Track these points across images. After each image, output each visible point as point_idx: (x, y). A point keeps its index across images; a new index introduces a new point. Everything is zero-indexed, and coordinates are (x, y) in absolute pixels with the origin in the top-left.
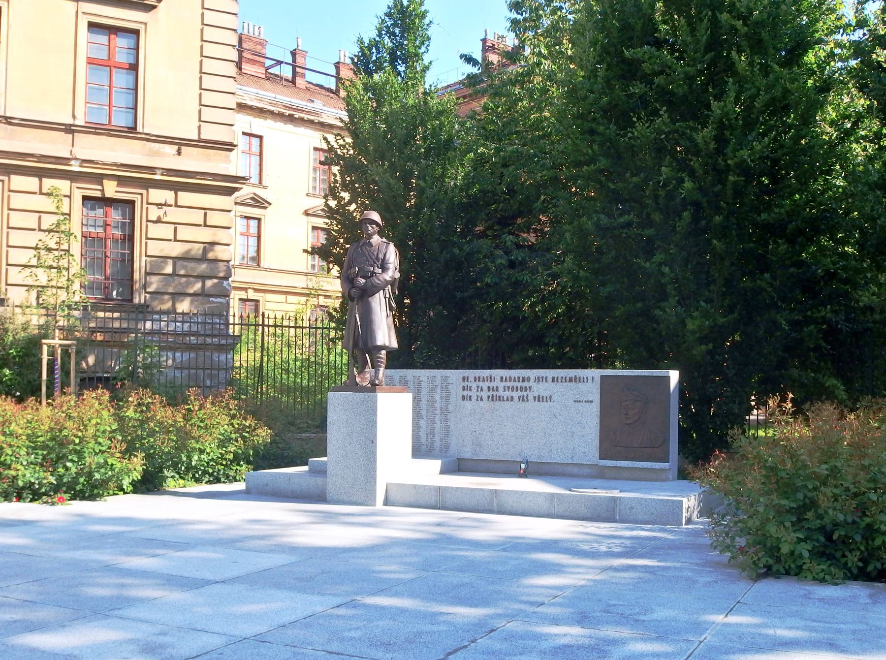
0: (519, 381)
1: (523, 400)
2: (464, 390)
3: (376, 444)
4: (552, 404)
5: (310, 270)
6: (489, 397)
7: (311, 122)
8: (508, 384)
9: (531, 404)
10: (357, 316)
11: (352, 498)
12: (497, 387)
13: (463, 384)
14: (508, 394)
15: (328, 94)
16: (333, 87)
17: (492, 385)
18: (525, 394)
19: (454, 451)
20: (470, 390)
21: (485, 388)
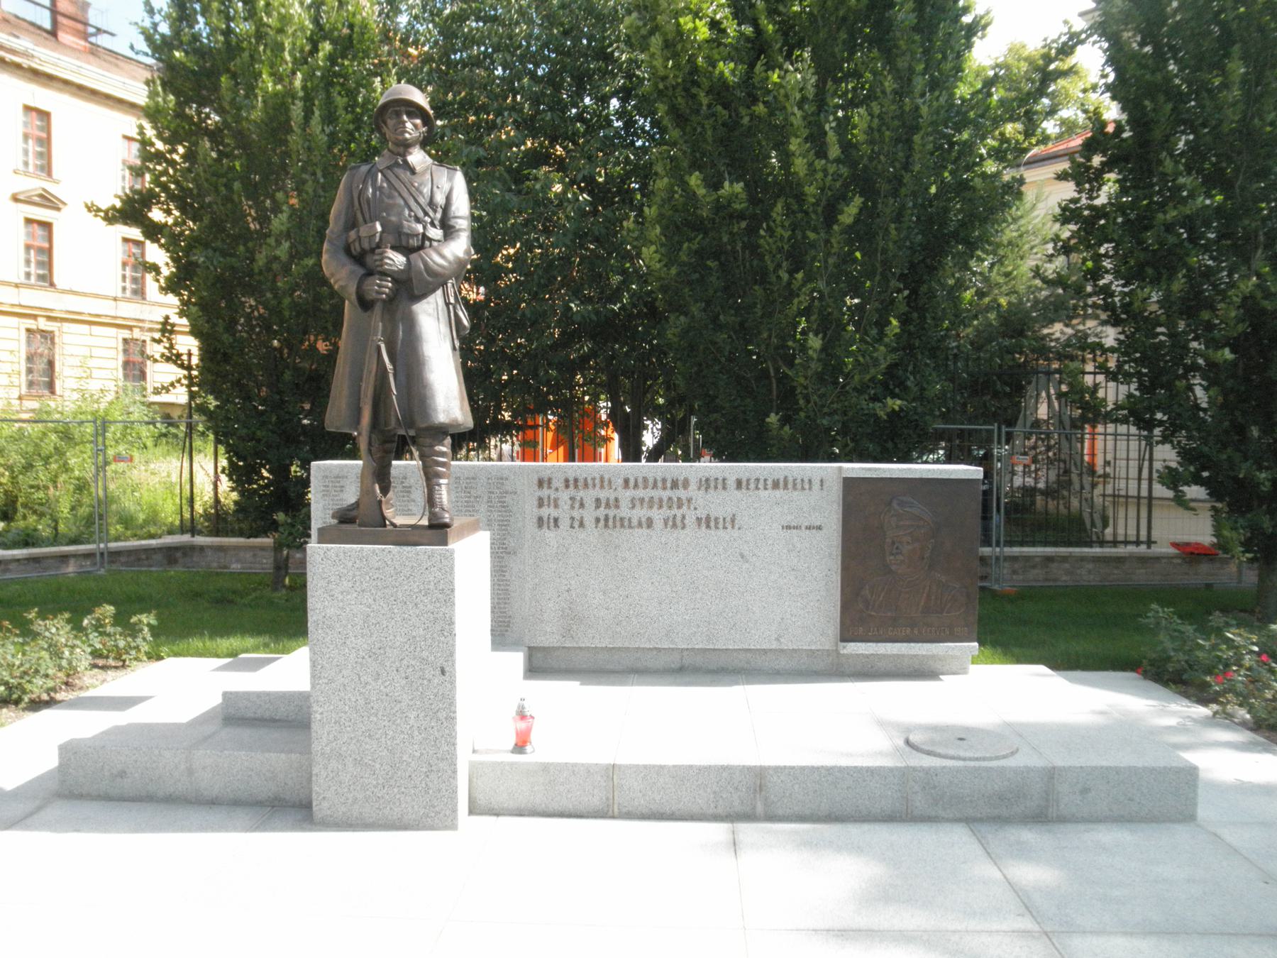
0: (665, 488)
1: (674, 525)
2: (541, 505)
3: (453, 676)
4: (736, 533)
5: (22, 279)
6: (598, 520)
7: (18, 66)
8: (640, 493)
9: (690, 534)
10: (383, 346)
11: (387, 811)
12: (617, 500)
13: (539, 493)
14: (640, 513)
15: (39, 32)
16: (47, 24)
17: (603, 494)
18: (679, 513)
19: (549, 636)
20: (556, 506)
21: (590, 503)
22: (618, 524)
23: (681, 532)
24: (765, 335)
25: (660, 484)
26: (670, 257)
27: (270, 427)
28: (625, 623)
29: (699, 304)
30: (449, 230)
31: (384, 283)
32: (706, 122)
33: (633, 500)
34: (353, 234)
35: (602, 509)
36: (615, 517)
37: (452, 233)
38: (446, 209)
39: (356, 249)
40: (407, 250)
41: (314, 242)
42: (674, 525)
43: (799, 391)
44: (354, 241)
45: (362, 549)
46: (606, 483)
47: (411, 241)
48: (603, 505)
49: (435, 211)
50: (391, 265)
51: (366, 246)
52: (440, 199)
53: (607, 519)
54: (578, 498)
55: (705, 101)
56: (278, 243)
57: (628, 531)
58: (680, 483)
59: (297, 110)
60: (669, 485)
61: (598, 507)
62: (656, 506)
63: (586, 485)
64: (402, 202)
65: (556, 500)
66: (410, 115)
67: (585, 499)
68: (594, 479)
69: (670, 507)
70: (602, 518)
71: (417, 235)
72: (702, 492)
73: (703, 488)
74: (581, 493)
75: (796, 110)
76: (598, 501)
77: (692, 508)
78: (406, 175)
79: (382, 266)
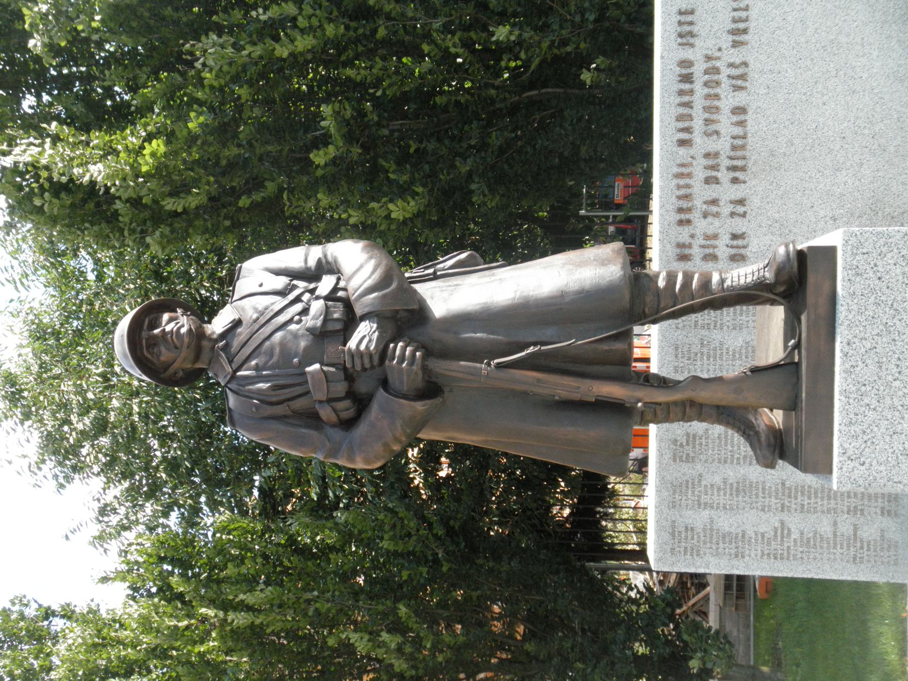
0: (691, 92)
6: (735, 181)
8: (698, 125)
12: (707, 155)
14: (725, 124)
17: (700, 174)
18: (726, 71)
20: (715, 237)
21: (711, 192)
22: (739, 153)
23: (751, 66)
24: (493, 92)
25: (686, 99)
26: (403, 191)
27: (589, 670)
28: (883, 141)
29: (458, 164)
30: (325, 268)
31: (398, 352)
32: (258, 151)
33: (707, 134)
34: (326, 413)
35: (719, 175)
36: (731, 158)
37: (328, 262)
38: (294, 275)
39: (346, 408)
40: (351, 321)
41: (383, 604)
42: (743, 77)
43: (556, 51)
44: (335, 410)
45: (844, 392)
46: (685, 170)
47: (336, 316)
48: (714, 173)
49: (295, 287)
50: (370, 341)
51: (341, 388)
52: (281, 282)
53: (734, 169)
54: (705, 206)
55: (235, 151)
56: (383, 644)
57: (750, 139)
58: (684, 71)
59: (239, 619)
60: (687, 86)
61: (716, 181)
62: (716, 103)
63: (687, 197)
64: (279, 335)
65: (707, 237)
66: (155, 324)
67: (705, 199)
68: (679, 187)
69: (718, 83)
70: (732, 174)
71: (327, 307)
72: (697, 42)
73: (691, 40)
74: (698, 203)
75: (245, 53)
76: (708, 181)
77: (718, 54)
78: (240, 334)
79: (371, 356)
